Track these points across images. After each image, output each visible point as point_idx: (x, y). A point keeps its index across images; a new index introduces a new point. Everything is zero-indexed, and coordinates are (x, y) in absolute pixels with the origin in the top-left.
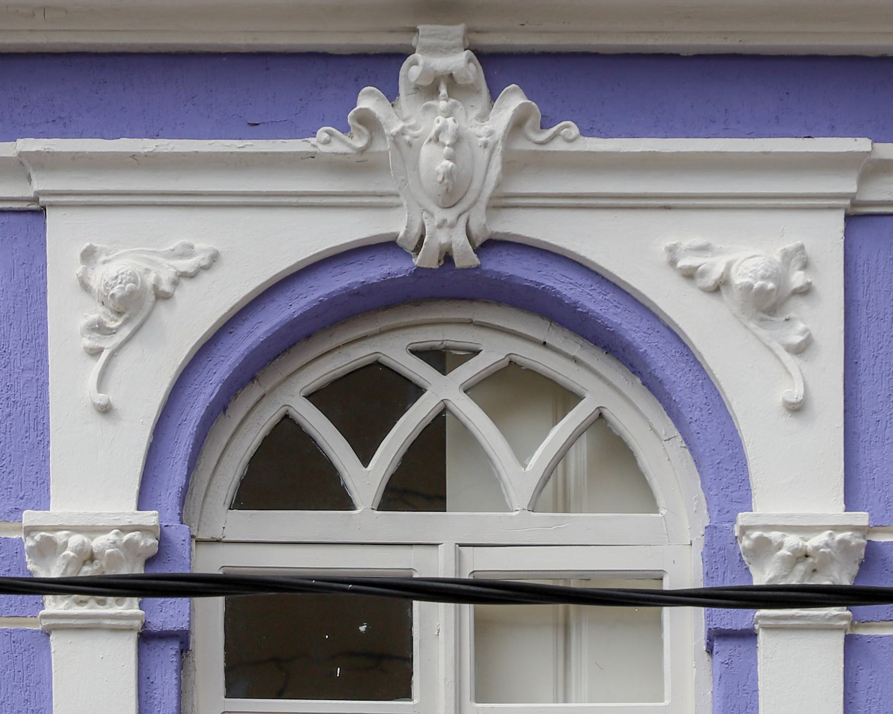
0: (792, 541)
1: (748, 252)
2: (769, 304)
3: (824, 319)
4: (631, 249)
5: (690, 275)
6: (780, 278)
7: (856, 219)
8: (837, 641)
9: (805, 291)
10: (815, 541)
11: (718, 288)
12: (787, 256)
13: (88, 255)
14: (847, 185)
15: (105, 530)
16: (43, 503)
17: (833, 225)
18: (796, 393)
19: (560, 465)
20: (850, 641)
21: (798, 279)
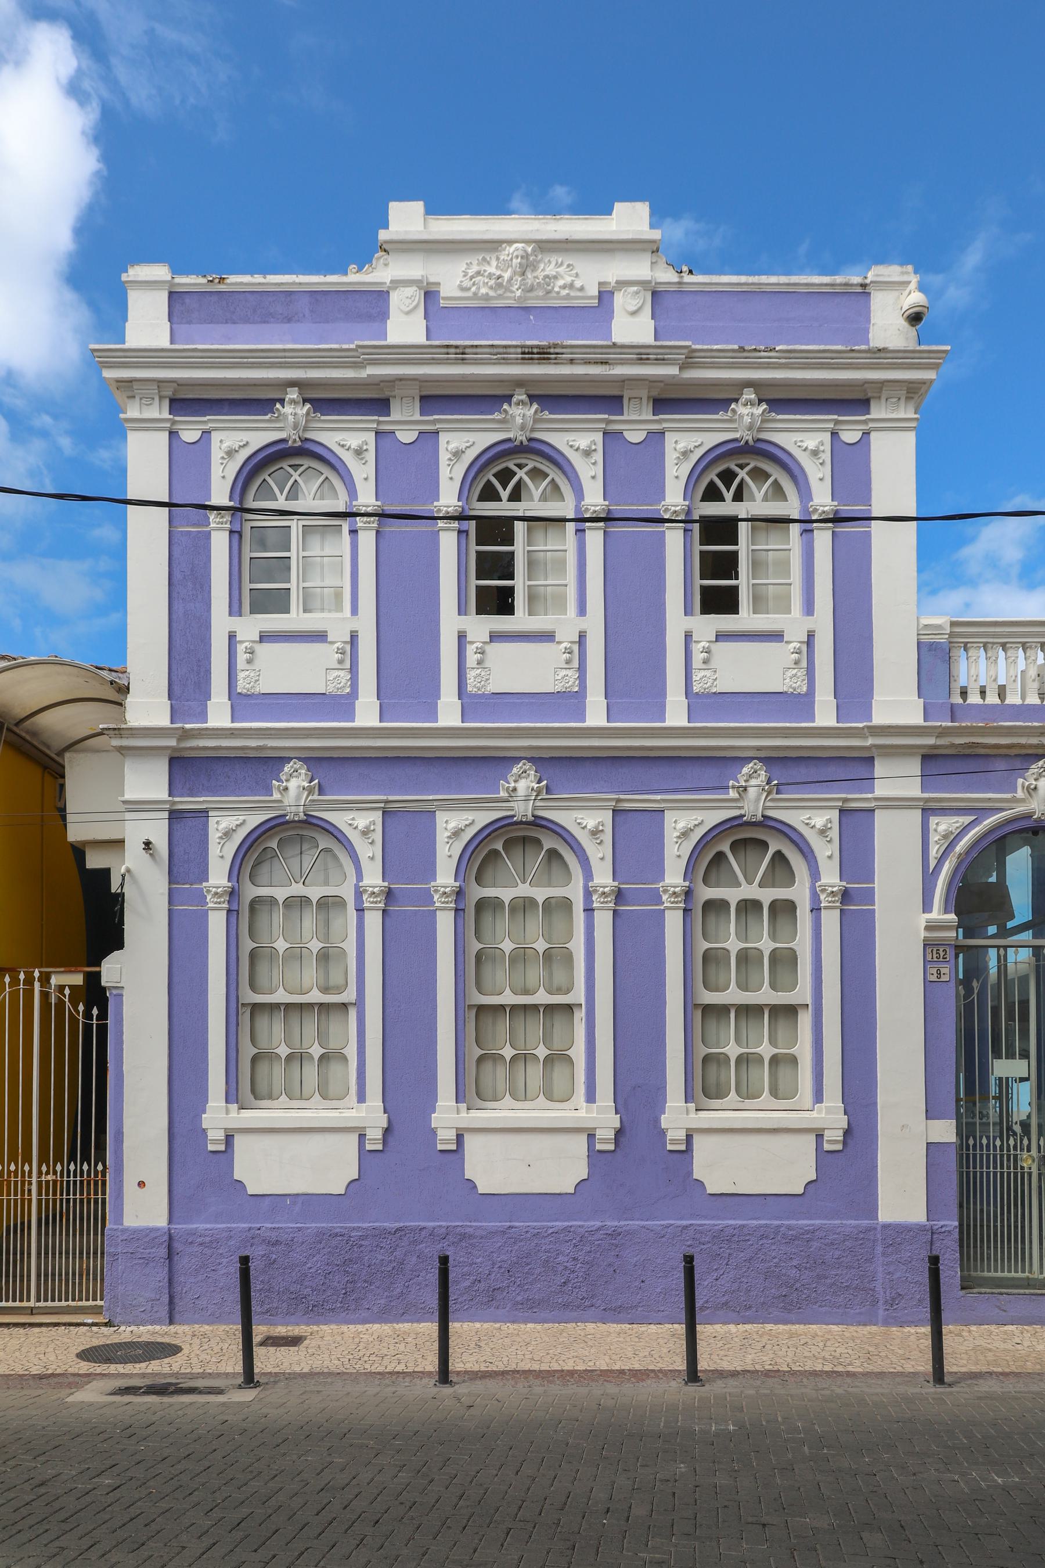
1: (819, 820)
2: (595, 833)
3: (834, 834)
5: (807, 824)
13: (937, 824)
19: (932, 864)
20: (615, 911)
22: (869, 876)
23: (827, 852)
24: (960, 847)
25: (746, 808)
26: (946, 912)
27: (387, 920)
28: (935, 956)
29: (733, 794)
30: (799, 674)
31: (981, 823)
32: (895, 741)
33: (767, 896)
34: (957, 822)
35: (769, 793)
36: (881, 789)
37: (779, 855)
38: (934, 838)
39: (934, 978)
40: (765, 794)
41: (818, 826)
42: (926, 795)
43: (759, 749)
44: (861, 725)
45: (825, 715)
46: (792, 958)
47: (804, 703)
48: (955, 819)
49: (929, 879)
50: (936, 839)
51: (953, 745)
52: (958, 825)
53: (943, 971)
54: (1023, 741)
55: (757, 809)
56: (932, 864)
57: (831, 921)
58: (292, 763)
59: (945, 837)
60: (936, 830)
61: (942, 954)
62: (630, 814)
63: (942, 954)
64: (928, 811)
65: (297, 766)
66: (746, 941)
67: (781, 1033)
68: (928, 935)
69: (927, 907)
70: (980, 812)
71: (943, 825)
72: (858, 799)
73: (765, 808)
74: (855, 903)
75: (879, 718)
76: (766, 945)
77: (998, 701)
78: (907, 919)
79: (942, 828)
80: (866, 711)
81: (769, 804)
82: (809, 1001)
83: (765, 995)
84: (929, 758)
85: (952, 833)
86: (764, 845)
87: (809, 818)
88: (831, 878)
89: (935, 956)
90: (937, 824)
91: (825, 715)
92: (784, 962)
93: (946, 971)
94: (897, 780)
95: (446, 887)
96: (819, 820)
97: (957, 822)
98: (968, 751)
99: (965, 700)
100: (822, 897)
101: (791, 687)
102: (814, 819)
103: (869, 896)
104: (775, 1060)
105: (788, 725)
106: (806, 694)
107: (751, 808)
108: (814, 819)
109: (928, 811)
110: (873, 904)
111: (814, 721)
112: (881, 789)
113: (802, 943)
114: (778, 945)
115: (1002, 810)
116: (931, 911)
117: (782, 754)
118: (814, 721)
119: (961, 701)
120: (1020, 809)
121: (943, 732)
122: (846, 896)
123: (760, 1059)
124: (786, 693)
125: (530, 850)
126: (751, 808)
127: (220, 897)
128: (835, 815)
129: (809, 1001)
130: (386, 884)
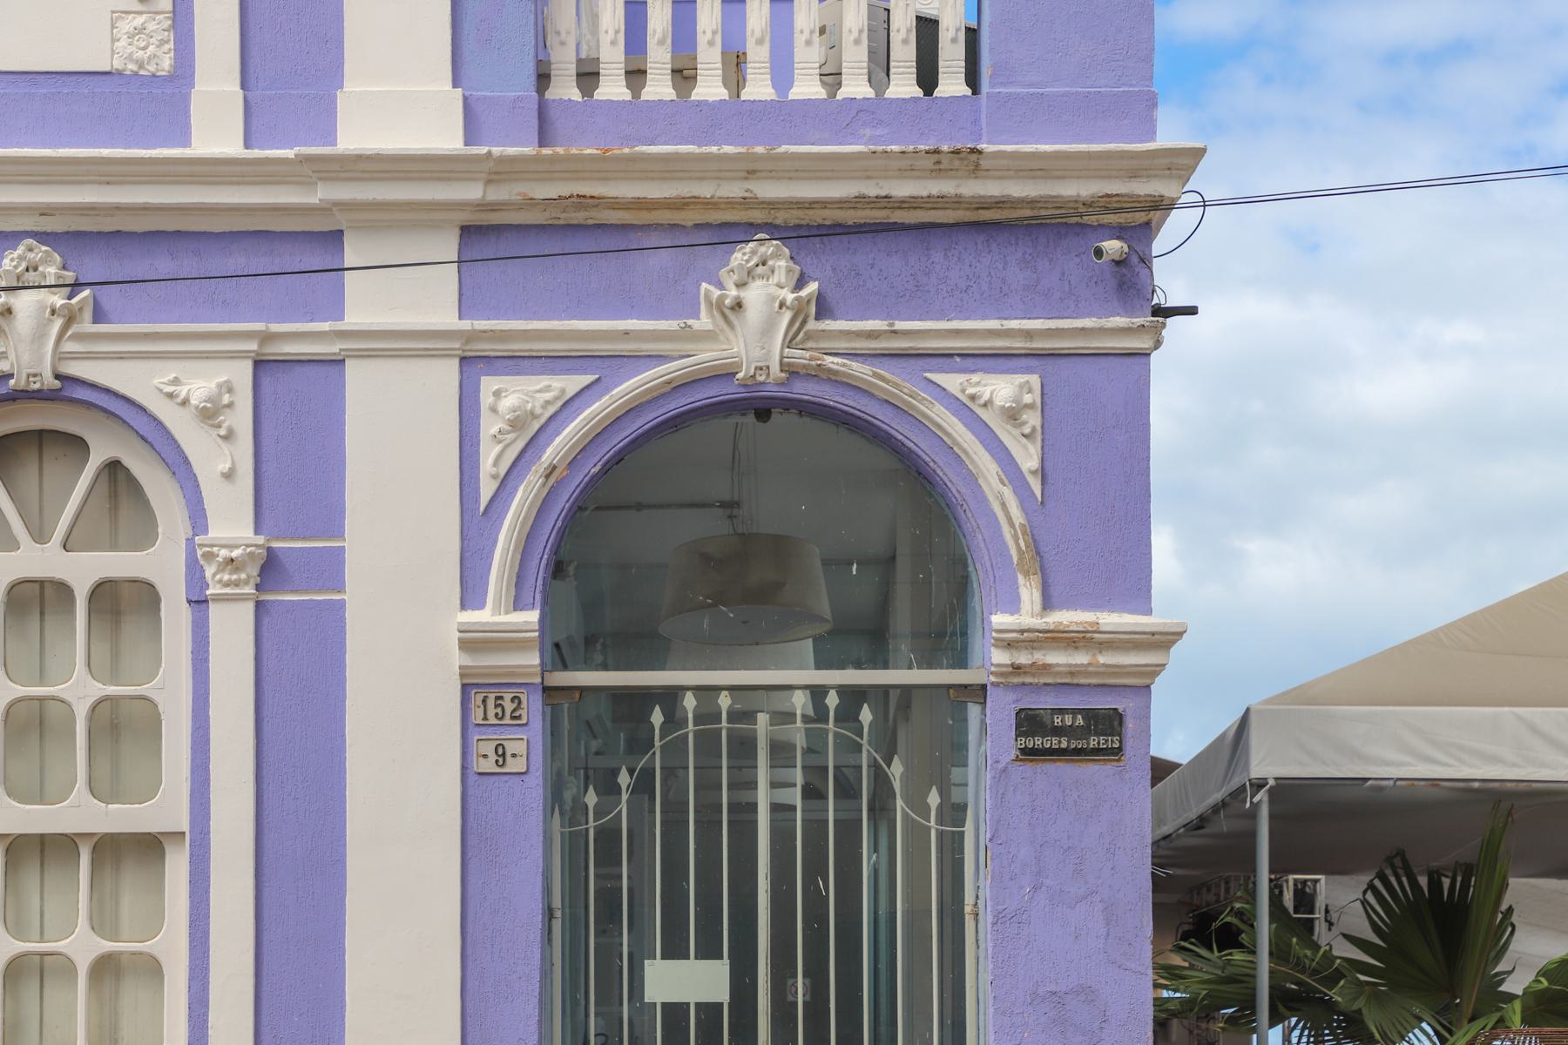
0: (224, 553)
1: (200, 385)
2: (209, 414)
3: (241, 418)
4: (138, 380)
5: (171, 396)
6: (1017, 400)
7: (259, 364)
8: (249, 607)
9: (230, 405)
10: (235, 553)
11: (185, 402)
12: (219, 386)
13: (497, 394)
14: (253, 346)
15: (237, 547)
16: (206, 531)
17: (247, 367)
18: (225, 466)
19: (487, 489)
20: (259, 605)
21: (226, 399)
22: (331, 520)
23: (222, 460)
24: (555, 449)
25: (12, 356)
26: (518, 606)
27: (266, 621)
28: (491, 711)
29: (704, 322)
30: (152, 26)
31: (607, 390)
32: (392, 192)
33: (83, 570)
34: (547, 389)
35: (70, 320)
36: (356, 316)
37: (114, 468)
38: (490, 427)
39: (488, 766)
40: (58, 323)
41: (998, 402)
42: (466, 325)
43: (46, 211)
44: (289, 153)
45: (216, 130)
46: (148, 721)
47: (162, 97)
48: (544, 381)
49: (476, 525)
50: (494, 430)
51: (531, 203)
52: (548, 396)
53: (511, 748)
54: (705, 190)
55: (41, 360)
56: (487, 489)
57: (233, 629)
58: (20, 250)
59: (516, 424)
60: (494, 410)
61: (509, 707)
62: (298, 368)
63: (509, 707)
64: (475, 363)
65: (35, 256)
66: (114, 678)
67: (130, 902)
68: (468, 661)
69: (471, 595)
70: (606, 363)
71: (511, 396)
72: (301, 336)
73: (59, 357)
74: (292, 586)
75: (352, 138)
76: (80, 689)
77: (869, 92)
78: (427, 621)
79: (508, 403)
80: (324, 120)
81: (69, 346)
82: (185, 826)
83: (79, 812)
84: (482, 237)
85: (534, 416)
86: (77, 446)
87: (176, 382)
88: (232, 526)
89: (491, 711)
90: (497, 394)
91: (216, 130)
92: (122, 729)
93: (520, 748)
94: (402, 291)
95: (232, 547)
96: (200, 385)
97: (547, 389)
98: (578, 217)
99: (636, 94)
100: (209, 571)
101: (130, 57)
102: (186, 381)
103: (330, 570)
104: (106, 969)
105: (106, 152)
106: (171, 78)
107: (26, 357)
108: (186, 381)
109: (475, 363)
110: (340, 588)
111: (186, 143)
112: (356, 316)
113: (170, 689)
114: (113, 690)
115: (661, 358)
116: (481, 606)
117: (108, 225)
118: (186, 143)
119: (575, 95)
120: (706, 356)
121: (501, 171)
122: (271, 569)
123: (67, 967)
124: (120, 73)
125: (54, 467)
126: (26, 357)
127: (237, 570)
128: (243, 373)
129: (185, 826)
130: (261, 540)
